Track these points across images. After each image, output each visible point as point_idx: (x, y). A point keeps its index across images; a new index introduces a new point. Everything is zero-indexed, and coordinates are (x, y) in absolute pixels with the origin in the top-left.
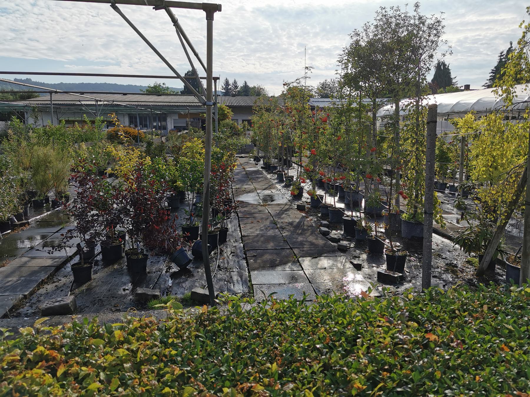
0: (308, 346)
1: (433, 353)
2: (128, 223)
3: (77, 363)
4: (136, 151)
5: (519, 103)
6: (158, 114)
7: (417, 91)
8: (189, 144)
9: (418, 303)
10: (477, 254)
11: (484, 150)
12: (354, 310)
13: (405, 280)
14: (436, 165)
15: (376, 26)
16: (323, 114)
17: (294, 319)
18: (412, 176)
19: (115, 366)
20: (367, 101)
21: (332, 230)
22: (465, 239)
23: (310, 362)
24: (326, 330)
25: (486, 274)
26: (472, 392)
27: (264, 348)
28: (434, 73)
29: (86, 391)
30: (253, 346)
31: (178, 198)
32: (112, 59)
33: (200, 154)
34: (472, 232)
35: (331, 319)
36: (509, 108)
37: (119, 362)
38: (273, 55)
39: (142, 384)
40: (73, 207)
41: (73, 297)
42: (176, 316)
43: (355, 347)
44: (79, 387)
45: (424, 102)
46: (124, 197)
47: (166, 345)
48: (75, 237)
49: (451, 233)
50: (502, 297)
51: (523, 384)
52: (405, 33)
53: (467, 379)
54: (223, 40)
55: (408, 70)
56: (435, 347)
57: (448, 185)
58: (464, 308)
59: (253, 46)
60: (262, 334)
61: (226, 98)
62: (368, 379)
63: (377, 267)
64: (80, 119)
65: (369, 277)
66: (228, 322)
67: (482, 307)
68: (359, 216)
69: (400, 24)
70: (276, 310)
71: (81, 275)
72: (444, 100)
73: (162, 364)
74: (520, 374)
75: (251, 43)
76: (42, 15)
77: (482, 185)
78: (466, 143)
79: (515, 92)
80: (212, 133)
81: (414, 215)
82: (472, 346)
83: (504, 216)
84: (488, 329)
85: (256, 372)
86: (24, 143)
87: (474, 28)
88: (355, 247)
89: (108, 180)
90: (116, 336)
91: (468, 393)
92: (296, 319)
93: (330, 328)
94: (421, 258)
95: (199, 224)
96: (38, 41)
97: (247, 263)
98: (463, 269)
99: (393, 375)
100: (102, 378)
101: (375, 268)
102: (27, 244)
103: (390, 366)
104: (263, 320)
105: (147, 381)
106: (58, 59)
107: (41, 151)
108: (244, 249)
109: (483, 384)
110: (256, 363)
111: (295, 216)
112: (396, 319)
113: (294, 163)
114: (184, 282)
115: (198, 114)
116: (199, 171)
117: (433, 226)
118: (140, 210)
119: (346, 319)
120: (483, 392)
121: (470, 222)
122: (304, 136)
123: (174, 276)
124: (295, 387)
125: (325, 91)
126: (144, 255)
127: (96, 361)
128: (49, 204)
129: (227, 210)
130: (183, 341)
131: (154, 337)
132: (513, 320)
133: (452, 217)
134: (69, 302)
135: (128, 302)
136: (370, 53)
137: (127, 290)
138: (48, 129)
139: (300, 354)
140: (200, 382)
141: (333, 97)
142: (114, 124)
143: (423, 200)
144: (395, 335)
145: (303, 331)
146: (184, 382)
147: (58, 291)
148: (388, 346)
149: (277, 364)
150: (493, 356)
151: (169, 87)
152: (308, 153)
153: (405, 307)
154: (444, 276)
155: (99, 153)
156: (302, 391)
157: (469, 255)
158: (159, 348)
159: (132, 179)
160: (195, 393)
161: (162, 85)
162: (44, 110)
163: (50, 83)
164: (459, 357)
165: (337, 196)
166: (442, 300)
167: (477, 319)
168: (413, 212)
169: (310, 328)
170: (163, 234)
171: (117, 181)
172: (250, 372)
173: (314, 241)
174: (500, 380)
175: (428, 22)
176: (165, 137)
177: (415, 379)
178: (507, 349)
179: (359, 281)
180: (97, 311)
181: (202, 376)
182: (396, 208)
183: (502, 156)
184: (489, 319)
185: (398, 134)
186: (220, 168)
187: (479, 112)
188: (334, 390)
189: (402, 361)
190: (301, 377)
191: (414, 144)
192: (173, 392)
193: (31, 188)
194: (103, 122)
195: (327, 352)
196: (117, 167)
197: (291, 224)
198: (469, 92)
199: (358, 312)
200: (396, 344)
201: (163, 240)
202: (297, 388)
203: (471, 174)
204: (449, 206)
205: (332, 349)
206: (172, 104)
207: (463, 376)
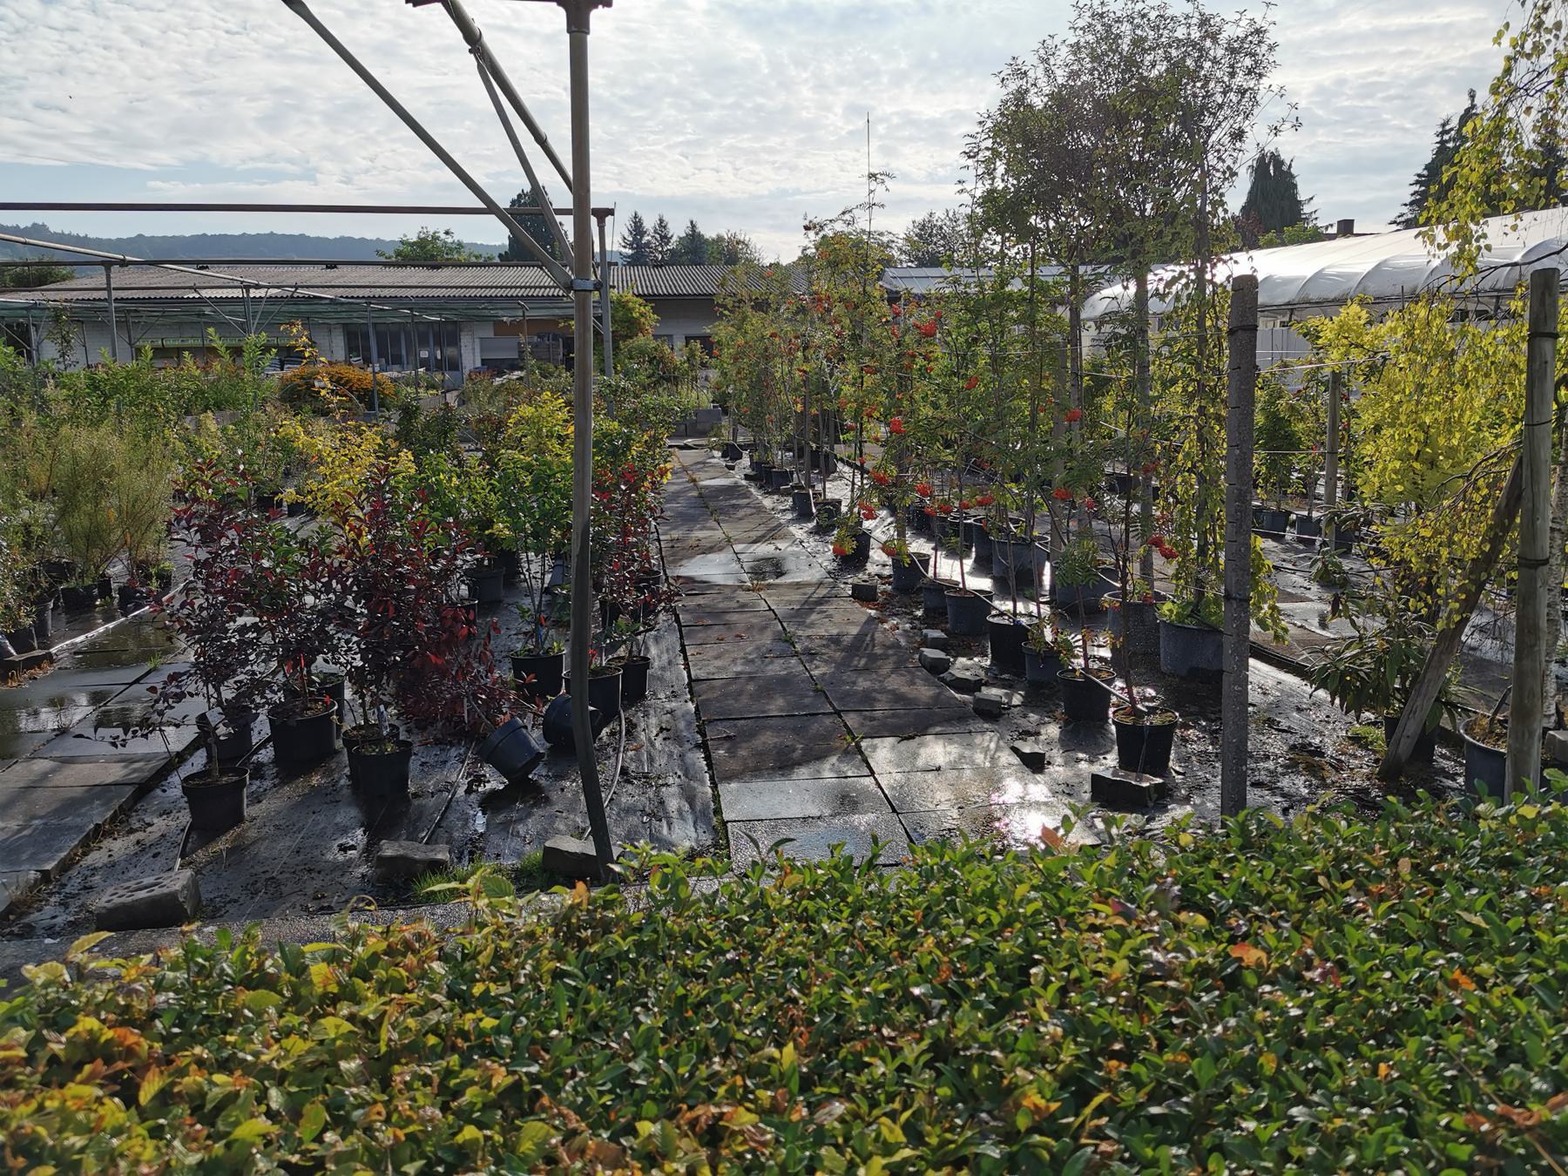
0: (888, 992)
2: (350, 649)
3: (200, 1062)
7: (1198, 240)
8: (527, 411)
9: (1207, 858)
11: (1394, 410)
12: (1021, 882)
13: (1171, 796)
14: (1258, 460)
15: (1076, 49)
16: (925, 316)
18: (1187, 492)
19: (313, 1069)
20: (1050, 272)
21: (955, 657)
23: (892, 1039)
24: (939, 944)
25: (1407, 772)
26: (1366, 1111)
27: (755, 1002)
28: (1248, 186)
29: (228, 1146)
30: (725, 998)
31: (499, 572)
32: (291, 161)
33: (562, 439)
34: (1363, 653)
35: (955, 910)
36: (1468, 286)
37: (326, 1057)
38: (773, 141)
39: (395, 1117)
40: (183, 606)
41: (188, 872)
42: (494, 916)
43: (1025, 991)
44: (205, 1132)
45: (1221, 273)
46: (334, 573)
47: (464, 1001)
48: (191, 695)
49: (1303, 657)
51: (1517, 1083)
52: (1162, 67)
54: (625, 99)
55: (1172, 176)
56: (1260, 985)
57: (1293, 517)
58: (1341, 866)
59: (712, 115)
61: (636, 272)
62: (1064, 1082)
63: (1091, 762)
64: (199, 343)
65: (1068, 790)
66: (651, 928)
67: (1395, 863)
68: (1035, 612)
69: (1145, 39)
71: (213, 806)
72: (1279, 266)
75: (706, 106)
76: (73, 30)
77: (1392, 515)
78: (1345, 391)
79: (1485, 236)
80: (594, 375)
81: (1196, 607)
82: (1366, 975)
83: (1457, 600)
84: (1412, 926)
85: (735, 1073)
86: (30, 419)
88: (1024, 704)
90: (316, 979)
91: (1357, 1115)
92: (851, 915)
93: (952, 939)
94: (1216, 731)
96: (64, 111)
97: (708, 758)
98: (1339, 761)
99: (1136, 1068)
100: (274, 1106)
101: (1083, 765)
102: (48, 720)
103: (1126, 1042)
105: (411, 1108)
106: (129, 163)
107: (82, 441)
108: (699, 719)
109: (1402, 1086)
110: (733, 1046)
111: (848, 618)
112: (1145, 906)
113: (842, 460)
114: (520, 820)
115: (553, 322)
116: (558, 491)
117: (1251, 638)
119: (997, 910)
120: (1400, 1110)
121: (1360, 621)
122: (869, 380)
123: (491, 803)
124: (849, 1112)
125: (929, 246)
126: (400, 743)
127: (256, 1054)
128: (112, 598)
129: (646, 603)
130: (517, 988)
131: (430, 980)
132: (1485, 898)
133: (1306, 611)
134: (177, 887)
135: (355, 883)
136: (1058, 130)
137: (353, 847)
138: (101, 374)
139: (864, 1016)
140: (569, 1107)
141: (951, 262)
142: (300, 355)
143: (1222, 561)
144: (1142, 952)
145: (873, 950)
146: (520, 1108)
148: (1122, 984)
149: (796, 1048)
150: (1428, 1005)
151: (465, 241)
153: (1170, 869)
154: (1285, 783)
155: (257, 443)
156: (870, 1124)
158: (445, 1012)
159: (358, 518)
160: (554, 1141)
161: (443, 236)
162: (88, 318)
163: (114, 237)
164: (1329, 1010)
165: (968, 556)
166: (1278, 846)
167: (1382, 898)
169: (891, 941)
170: (454, 678)
171: (314, 526)
172: (717, 1073)
173: (904, 689)
174: (1448, 1073)
175: (1229, 32)
176: (455, 393)
178: (1468, 985)
179: (1037, 803)
180: (263, 913)
181: (574, 1088)
182: (1141, 587)
183: (1449, 425)
184: (1416, 897)
185: (1144, 367)
186: (622, 479)
187: (1380, 300)
188: (965, 1116)
189: (1163, 1028)
190: (869, 1082)
191: (1191, 396)
192: (487, 1138)
194: (266, 349)
195: (943, 1009)
197: (835, 640)
199: (1034, 888)
200: (1146, 978)
201: (457, 699)
202: (856, 1116)
203: (1359, 482)
204: (1297, 578)
205: (958, 997)
206: (473, 292)
207: (1340, 1065)
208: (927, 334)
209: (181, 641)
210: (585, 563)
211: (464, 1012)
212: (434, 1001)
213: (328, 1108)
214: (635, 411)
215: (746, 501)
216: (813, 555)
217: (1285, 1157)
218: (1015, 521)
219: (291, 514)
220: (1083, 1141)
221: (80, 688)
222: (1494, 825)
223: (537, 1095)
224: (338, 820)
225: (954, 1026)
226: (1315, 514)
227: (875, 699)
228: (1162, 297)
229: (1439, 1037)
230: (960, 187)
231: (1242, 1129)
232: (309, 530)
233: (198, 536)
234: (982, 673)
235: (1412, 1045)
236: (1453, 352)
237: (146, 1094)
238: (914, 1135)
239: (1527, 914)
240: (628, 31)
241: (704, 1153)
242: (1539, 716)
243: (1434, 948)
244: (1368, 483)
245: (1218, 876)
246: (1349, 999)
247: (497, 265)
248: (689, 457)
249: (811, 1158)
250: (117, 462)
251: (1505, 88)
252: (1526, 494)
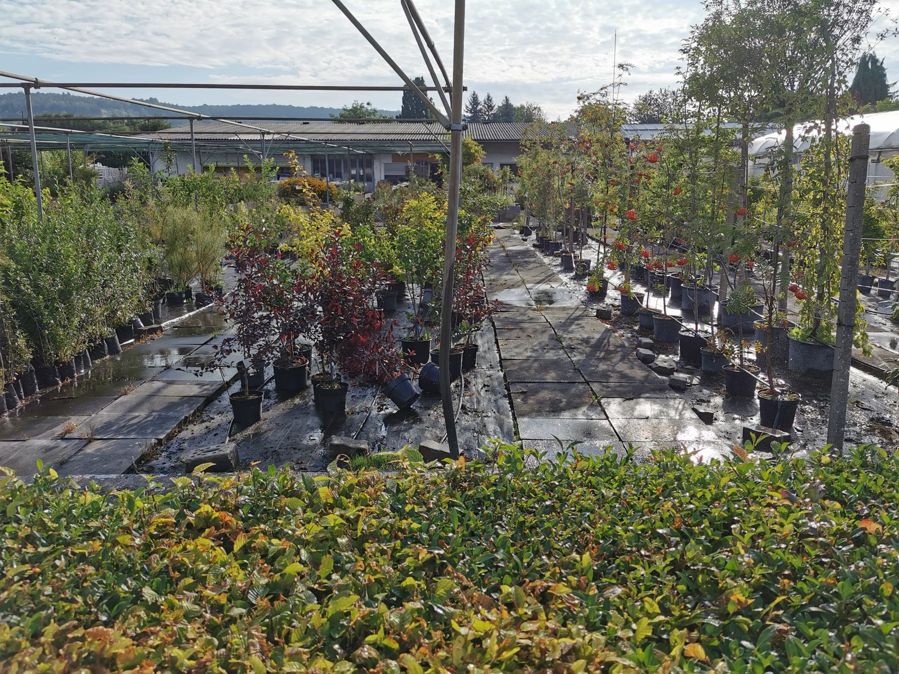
3: (264, 533)
8: (414, 203)
19: (322, 540)
21: (658, 354)
23: (648, 556)
27: (565, 529)
32: (285, 64)
37: (329, 535)
38: (556, 49)
39: (368, 569)
41: (233, 445)
44: (269, 568)
47: (402, 515)
49: (882, 365)
57: (876, 280)
59: (521, 34)
62: (756, 588)
65: (728, 436)
66: (502, 484)
71: (245, 412)
75: (516, 29)
81: (814, 332)
90: (322, 495)
94: (823, 407)
96: (168, 36)
97: (511, 403)
99: (800, 585)
100: (303, 558)
101: (737, 422)
102: (159, 361)
107: (178, 215)
111: (594, 329)
114: (406, 431)
115: (425, 154)
116: (431, 248)
118: (336, 310)
122: (612, 190)
123: (389, 420)
125: (650, 111)
126: (341, 384)
127: (294, 531)
130: (429, 510)
134: (228, 452)
139: (630, 542)
145: (632, 507)
147: (210, 436)
151: (378, 109)
160: (455, 590)
161: (366, 106)
168: (811, 326)
173: (627, 371)
189: (817, 564)
196: (296, 241)
197: (586, 341)
199: (731, 480)
200: (804, 535)
201: (372, 362)
204: (877, 318)
211: (401, 520)
215: (533, 259)
220: (768, 623)
221: (174, 347)
223: (443, 566)
224: (309, 423)
227: (610, 377)
231: (873, 624)
245: (848, 481)
248: (499, 234)
249: (603, 616)
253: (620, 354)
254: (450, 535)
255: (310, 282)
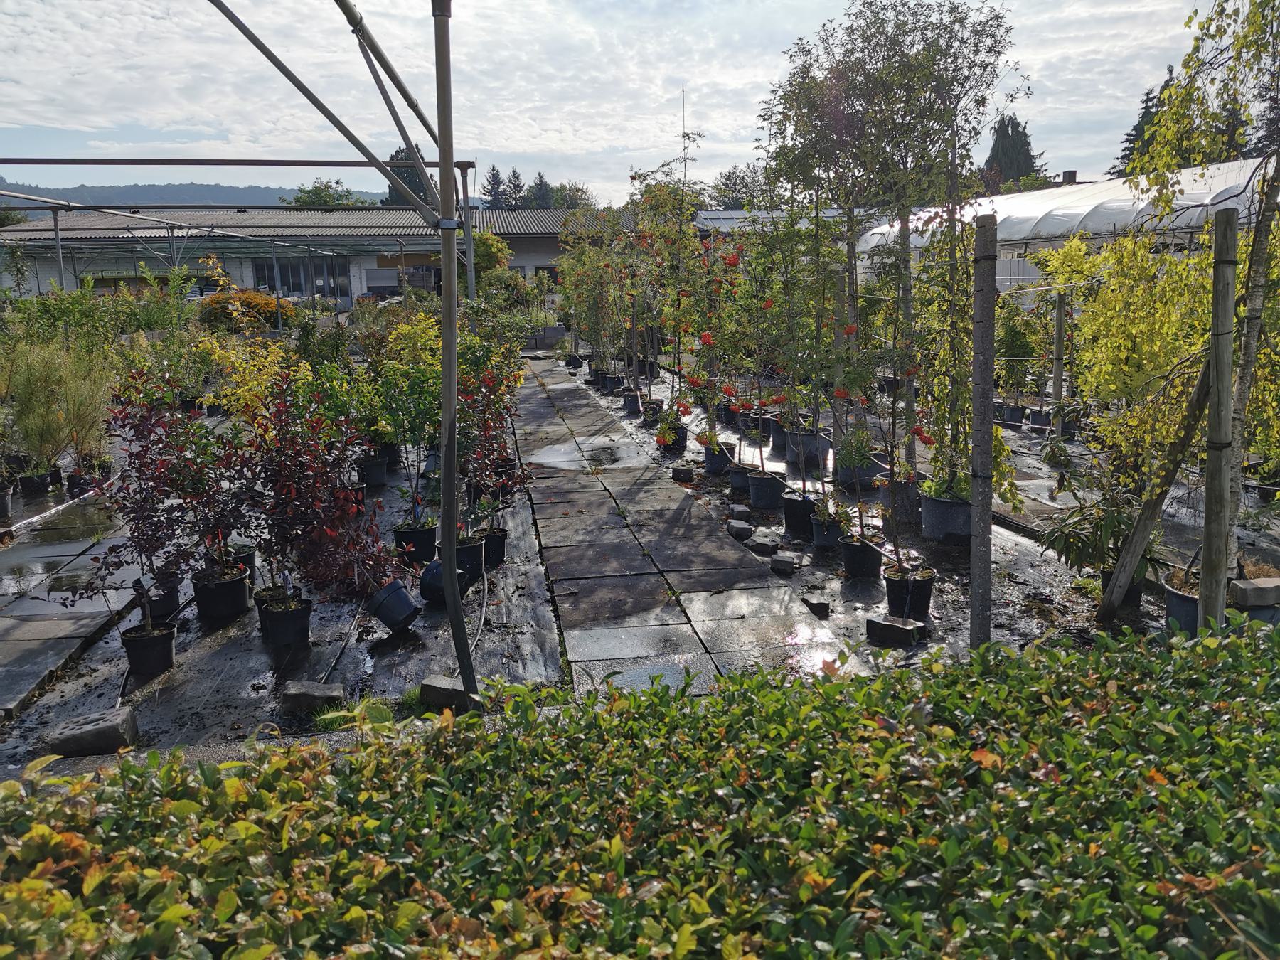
0: (697, 794)
1: (991, 795)
2: (259, 525)
3: (134, 860)
4: (273, 348)
5: (1187, 208)
6: (326, 256)
7: (949, 187)
8: (405, 328)
9: (955, 683)
10: (1098, 569)
11: (1107, 324)
12: (805, 704)
14: (999, 365)
17: (663, 732)
18: (942, 391)
20: (832, 213)
21: (756, 527)
22: (1068, 537)
23: (700, 831)
25: (1119, 613)
26: (1080, 881)
27: (589, 804)
29: (157, 927)
30: (565, 800)
31: (382, 463)
32: (208, 124)
37: (237, 854)
38: (606, 107)
39: (294, 901)
40: (120, 490)
41: (127, 709)
42: (376, 738)
43: (807, 791)
44: (138, 916)
45: (968, 214)
46: (245, 462)
47: (351, 807)
48: (128, 564)
49: (1035, 523)
50: (1150, 662)
53: (1070, 852)
54: (483, 72)
56: (995, 782)
57: (1028, 411)
58: (1061, 688)
59: (556, 86)
60: (586, 771)
61: (494, 215)
62: (838, 862)
64: (132, 274)
66: (504, 745)
67: (1104, 685)
68: (821, 490)
69: (906, 24)
70: (621, 715)
71: (148, 655)
72: (1015, 208)
73: (343, 854)
74: (1189, 834)
75: (549, 78)
77: (1108, 409)
79: (1178, 182)
81: (951, 484)
83: (1158, 477)
84: (1118, 735)
85: (573, 860)
87: (1082, 34)
88: (812, 564)
89: (208, 422)
90: (229, 791)
92: (668, 732)
94: (966, 584)
95: (433, 520)
96: (17, 82)
97: (555, 611)
99: (895, 850)
100: (195, 894)
101: (860, 613)
103: (888, 830)
104: (588, 739)
105: (308, 893)
106: (73, 125)
107: (35, 356)
110: (571, 839)
111: (669, 496)
112: (904, 721)
114: (401, 663)
116: (431, 394)
119: (785, 726)
120: (1107, 880)
121: (1080, 494)
122: (685, 302)
123: (377, 649)
124: (664, 889)
125: (734, 192)
126: (301, 601)
128: (62, 485)
130: (395, 796)
131: (324, 790)
134: (119, 720)
136: (836, 98)
137: (264, 687)
138: (51, 300)
139: (678, 813)
140: (437, 890)
141: (752, 206)
142: (216, 283)
143: (970, 447)
145: (686, 760)
148: (885, 784)
149: (622, 839)
150: (1129, 797)
151: (353, 189)
152: (697, 344)
154: (1021, 625)
155: (181, 357)
156: (682, 899)
157: (1080, 572)
158: (335, 815)
159: (265, 417)
160: (424, 918)
161: (334, 185)
163: (60, 187)
164: (1051, 802)
165: (766, 445)
166: (1011, 672)
167: (1094, 713)
168: (946, 477)
169: (700, 752)
171: (229, 424)
172: (558, 860)
173: (715, 553)
174: (1146, 850)
175: (973, 18)
176: (346, 315)
177: (949, 859)
179: (823, 643)
180: (191, 741)
181: (442, 875)
183: (1152, 335)
185: (907, 290)
186: (483, 385)
187: (1097, 236)
188: (759, 891)
190: (681, 866)
191: (945, 313)
192: (370, 916)
193: (14, 447)
194: (187, 279)
195: (741, 806)
197: (659, 514)
198: (1075, 187)
199: (815, 708)
200: (904, 778)
201: (349, 565)
202: (671, 892)
204: (1031, 461)
205: (754, 797)
206: (360, 232)
207: (1059, 846)
208: (732, 264)
209: (120, 520)
210: (452, 453)
211: (352, 816)
212: (327, 807)
213: (239, 894)
214: (494, 328)
215: (585, 402)
216: (641, 445)
217: (1014, 919)
218: (804, 417)
219: (210, 415)
220: (853, 909)
221: (36, 559)
222: (1184, 653)
224: (251, 665)
225: (750, 819)
226: (1045, 409)
227: (692, 562)
228: (921, 233)
229: (1138, 822)
230: (757, 144)
231: (980, 898)
232: (224, 428)
233: (132, 432)
234: (778, 540)
235: (1116, 828)
236: (1154, 276)
237: (89, 885)
238: (717, 906)
239: (1209, 723)
240: (486, 17)
241: (547, 925)
242: (1224, 569)
243: (1135, 751)
244: (1088, 383)
246: (1067, 793)
247: (379, 209)
248: (539, 366)
249: (634, 927)
250: (64, 373)
251: (1194, 63)
252: (1213, 390)
253: (704, 529)
254: (426, 831)
255: (248, 452)
